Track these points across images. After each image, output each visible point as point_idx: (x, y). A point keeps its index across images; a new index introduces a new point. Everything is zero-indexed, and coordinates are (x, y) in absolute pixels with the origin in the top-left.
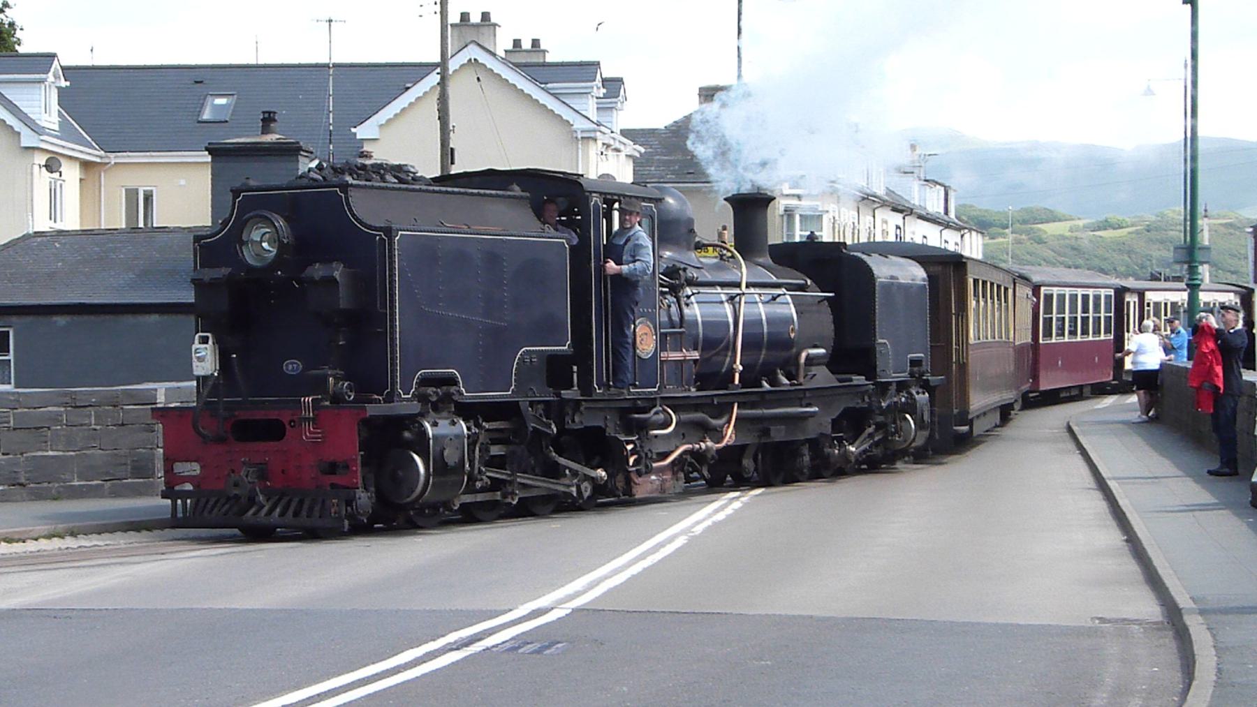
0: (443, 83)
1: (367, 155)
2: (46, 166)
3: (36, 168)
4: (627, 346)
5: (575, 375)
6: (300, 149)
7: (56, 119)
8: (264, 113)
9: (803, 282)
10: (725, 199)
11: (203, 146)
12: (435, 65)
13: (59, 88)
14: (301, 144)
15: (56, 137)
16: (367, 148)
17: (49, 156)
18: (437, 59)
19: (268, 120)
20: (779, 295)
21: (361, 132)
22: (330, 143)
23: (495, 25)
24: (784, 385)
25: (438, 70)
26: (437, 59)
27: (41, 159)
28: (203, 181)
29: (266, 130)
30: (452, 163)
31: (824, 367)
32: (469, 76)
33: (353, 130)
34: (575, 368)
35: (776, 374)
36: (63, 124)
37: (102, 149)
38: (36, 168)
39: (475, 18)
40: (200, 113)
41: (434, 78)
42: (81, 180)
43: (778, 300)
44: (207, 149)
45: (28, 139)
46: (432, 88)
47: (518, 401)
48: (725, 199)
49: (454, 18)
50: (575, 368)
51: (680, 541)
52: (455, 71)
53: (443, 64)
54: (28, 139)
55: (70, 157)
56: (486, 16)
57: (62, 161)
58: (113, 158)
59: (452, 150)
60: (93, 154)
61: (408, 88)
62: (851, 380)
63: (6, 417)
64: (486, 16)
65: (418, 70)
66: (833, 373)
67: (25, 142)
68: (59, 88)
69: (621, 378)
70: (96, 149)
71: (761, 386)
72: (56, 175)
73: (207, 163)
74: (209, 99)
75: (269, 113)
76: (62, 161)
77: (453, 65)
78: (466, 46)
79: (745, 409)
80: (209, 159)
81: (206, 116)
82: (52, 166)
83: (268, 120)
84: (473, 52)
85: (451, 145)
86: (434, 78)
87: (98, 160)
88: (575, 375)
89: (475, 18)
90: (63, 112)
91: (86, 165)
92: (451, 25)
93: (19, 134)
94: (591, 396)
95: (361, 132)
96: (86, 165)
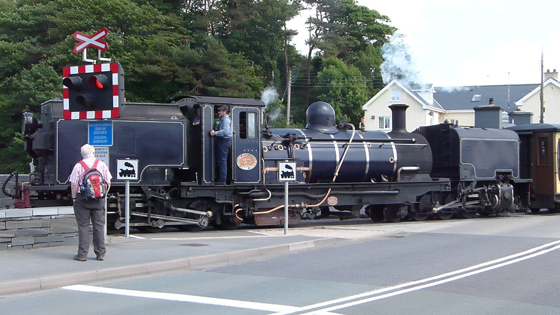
0: (542, 89)
1: (519, 110)
2: (430, 114)
3: (427, 114)
4: (224, 163)
5: (197, 176)
6: (500, 108)
7: (433, 101)
8: (490, 98)
9: (411, 140)
10: (389, 107)
11: (473, 107)
12: (540, 84)
13: (433, 93)
14: (500, 107)
15: (432, 106)
16: (519, 108)
17: (430, 111)
18: (540, 83)
19: (491, 101)
20: (382, 145)
21: (517, 103)
22: (508, 106)
23: (557, 73)
24: (385, 181)
25: (540, 86)
26: (540, 83)
27: (428, 112)
28: (473, 117)
29: (490, 104)
30: (544, 111)
31: (428, 174)
32: (549, 88)
33: (515, 103)
34: (196, 173)
35: (381, 177)
36: (434, 103)
37: (444, 109)
38: (427, 114)
39: (551, 71)
40: (472, 99)
41: (539, 88)
42: (439, 117)
43: (382, 147)
44: (474, 109)
45: (425, 107)
46: (539, 91)
47: (141, 186)
48: (389, 107)
49: (545, 71)
50: (196, 173)
51: (311, 245)
52: (545, 86)
53: (542, 84)
54: (425, 107)
55: (436, 112)
56: (554, 70)
57: (434, 113)
58: (448, 112)
59: (544, 108)
60: (442, 111)
61: (531, 91)
62: (438, 180)
63: (123, 184)
64: (554, 70)
65: (535, 86)
66: (431, 177)
67: (424, 108)
68: (433, 93)
69: (221, 177)
70: (442, 109)
71: (371, 181)
72: (432, 116)
73: (473, 113)
74: (474, 95)
75: (491, 98)
76: (434, 113)
77: (545, 84)
78: (549, 79)
79: (292, 192)
80: (474, 111)
81: (473, 100)
82: (431, 114)
83: (491, 101)
84: (551, 80)
85: (544, 107)
86: (539, 88)
87: (443, 112)
88: (197, 176)
89: (551, 71)
90: (435, 100)
91: (440, 113)
92: (545, 73)
93: (422, 105)
94: (201, 184)
95: (517, 103)
96: (440, 113)
